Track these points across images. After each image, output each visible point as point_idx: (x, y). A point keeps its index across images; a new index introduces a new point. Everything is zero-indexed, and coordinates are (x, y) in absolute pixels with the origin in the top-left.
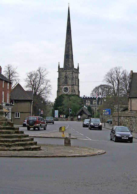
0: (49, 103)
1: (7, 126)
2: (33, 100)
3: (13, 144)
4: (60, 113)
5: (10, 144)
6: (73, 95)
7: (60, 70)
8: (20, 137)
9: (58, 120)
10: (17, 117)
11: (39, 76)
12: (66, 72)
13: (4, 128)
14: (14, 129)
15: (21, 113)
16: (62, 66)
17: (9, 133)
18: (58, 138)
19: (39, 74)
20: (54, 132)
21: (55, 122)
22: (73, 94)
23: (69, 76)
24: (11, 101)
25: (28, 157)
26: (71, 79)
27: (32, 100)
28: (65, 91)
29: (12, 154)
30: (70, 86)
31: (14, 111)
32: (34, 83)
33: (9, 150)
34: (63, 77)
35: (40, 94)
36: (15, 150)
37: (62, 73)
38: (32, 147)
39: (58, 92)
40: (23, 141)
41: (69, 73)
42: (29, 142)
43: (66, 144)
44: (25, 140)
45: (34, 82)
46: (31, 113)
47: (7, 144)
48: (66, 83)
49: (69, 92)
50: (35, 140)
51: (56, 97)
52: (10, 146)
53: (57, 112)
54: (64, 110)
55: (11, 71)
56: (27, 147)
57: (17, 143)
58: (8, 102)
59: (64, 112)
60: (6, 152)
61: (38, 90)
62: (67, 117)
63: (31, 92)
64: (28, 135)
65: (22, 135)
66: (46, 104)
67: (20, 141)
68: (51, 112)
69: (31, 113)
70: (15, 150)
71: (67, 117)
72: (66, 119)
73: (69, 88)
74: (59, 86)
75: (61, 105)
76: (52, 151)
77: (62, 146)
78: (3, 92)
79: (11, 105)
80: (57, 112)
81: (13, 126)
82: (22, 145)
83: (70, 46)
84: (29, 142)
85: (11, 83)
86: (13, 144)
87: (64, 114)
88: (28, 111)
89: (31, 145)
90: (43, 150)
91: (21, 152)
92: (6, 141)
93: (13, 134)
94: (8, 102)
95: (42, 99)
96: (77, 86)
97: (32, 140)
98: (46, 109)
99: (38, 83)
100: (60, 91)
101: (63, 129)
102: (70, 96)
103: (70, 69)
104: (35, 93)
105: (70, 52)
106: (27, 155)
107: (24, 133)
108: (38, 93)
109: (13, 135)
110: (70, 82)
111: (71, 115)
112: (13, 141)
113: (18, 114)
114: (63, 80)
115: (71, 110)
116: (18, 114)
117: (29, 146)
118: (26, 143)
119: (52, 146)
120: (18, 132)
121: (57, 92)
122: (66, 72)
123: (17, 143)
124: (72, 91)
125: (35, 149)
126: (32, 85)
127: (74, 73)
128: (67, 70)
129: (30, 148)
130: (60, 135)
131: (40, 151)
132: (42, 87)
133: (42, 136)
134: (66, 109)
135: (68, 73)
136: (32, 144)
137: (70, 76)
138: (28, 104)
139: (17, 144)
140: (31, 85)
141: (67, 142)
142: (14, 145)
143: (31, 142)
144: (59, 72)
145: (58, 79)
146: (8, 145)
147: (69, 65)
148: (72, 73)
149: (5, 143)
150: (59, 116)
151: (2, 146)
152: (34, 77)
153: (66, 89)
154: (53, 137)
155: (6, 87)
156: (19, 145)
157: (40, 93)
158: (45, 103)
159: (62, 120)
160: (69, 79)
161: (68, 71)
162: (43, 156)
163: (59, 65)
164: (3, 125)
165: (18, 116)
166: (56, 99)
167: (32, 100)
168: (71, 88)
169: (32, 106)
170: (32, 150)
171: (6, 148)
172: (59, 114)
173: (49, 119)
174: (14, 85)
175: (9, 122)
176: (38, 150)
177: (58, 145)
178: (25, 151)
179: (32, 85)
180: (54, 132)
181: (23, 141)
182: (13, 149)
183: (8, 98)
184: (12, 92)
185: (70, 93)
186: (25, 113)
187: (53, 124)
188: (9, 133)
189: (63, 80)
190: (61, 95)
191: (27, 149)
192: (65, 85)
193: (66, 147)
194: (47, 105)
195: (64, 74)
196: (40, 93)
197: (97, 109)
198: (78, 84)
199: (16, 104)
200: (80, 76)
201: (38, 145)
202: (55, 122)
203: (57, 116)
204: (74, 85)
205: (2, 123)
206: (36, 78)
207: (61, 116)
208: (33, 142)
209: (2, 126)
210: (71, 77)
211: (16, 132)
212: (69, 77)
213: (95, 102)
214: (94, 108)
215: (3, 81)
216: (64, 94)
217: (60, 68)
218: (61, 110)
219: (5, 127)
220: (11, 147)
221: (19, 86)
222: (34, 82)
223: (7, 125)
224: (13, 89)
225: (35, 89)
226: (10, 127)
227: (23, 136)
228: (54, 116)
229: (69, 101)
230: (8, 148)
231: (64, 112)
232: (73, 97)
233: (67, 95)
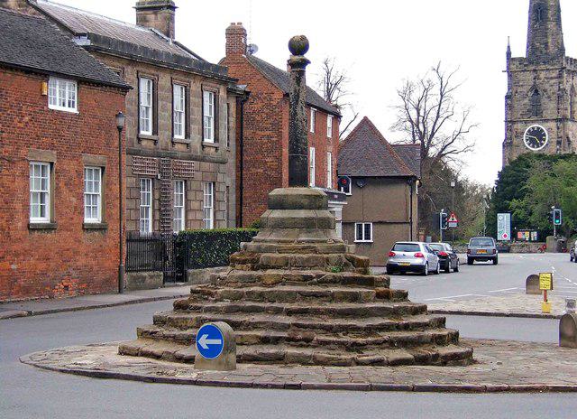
0: (474, 189)
1: (347, 274)
2: (418, 177)
3: (370, 339)
4: (516, 225)
5: (360, 340)
6: (565, 157)
7: (514, 67)
8: (395, 313)
9: (508, 251)
10: (363, 240)
11: (436, 90)
12: (535, 70)
13: (334, 281)
14: (370, 282)
15: (377, 226)
16: (520, 51)
17: (355, 298)
18: (525, 316)
19: (436, 81)
20: (506, 295)
21: (501, 257)
22: (563, 153)
23: (547, 86)
24: (341, 182)
25: (429, 391)
27: (416, 178)
28: (533, 142)
29: (371, 379)
30: (553, 125)
31: (351, 219)
32: (419, 115)
33: (358, 363)
34: (525, 90)
35: (441, 155)
36: (379, 363)
37: (521, 76)
38: (445, 351)
39: (507, 145)
40: (406, 327)
41: (547, 77)
42: (430, 333)
43: (564, 342)
44: (416, 323)
45: (418, 113)
46: (415, 225)
47: (348, 339)
48: (536, 111)
49: (548, 146)
50: (452, 324)
51: (498, 166)
52: (417, 342)
53: (504, 220)
54: (531, 214)
55: (333, 73)
56: (424, 351)
57: (386, 335)
58: (329, 185)
59: (532, 219)
60: (346, 369)
61: (434, 141)
62: (541, 238)
63: (412, 147)
64: (426, 307)
65: (403, 304)
66: (463, 190)
67: (398, 328)
68: (482, 220)
69: (415, 225)
70: (379, 363)
71: (541, 238)
72: (540, 245)
73: (550, 130)
74: (510, 123)
75: (520, 197)
76: (520, 367)
77: (549, 346)
78: (312, 150)
79: (342, 198)
80: (504, 220)
81: (366, 272)
82: (404, 343)
84: (430, 333)
85: (337, 117)
86: (370, 339)
87: (531, 227)
88: (400, 216)
89: (439, 344)
90: (482, 363)
91: (402, 370)
92: (346, 330)
93: (369, 301)
94: (329, 185)
95: (448, 174)
97: (441, 323)
98: (463, 209)
99: (433, 115)
100: (515, 141)
101: (544, 284)
102: (555, 158)
103: (549, 60)
104: (424, 151)
106: (429, 383)
107: (409, 298)
108: (433, 152)
109: (368, 305)
110: (550, 108)
111: (560, 231)
112: (370, 330)
113: (367, 227)
114: (526, 101)
115: (557, 214)
116: (367, 227)
117: (431, 347)
118: (420, 337)
119: (513, 346)
120: (386, 296)
122: (535, 70)
123: (386, 335)
124: (559, 143)
125: (456, 359)
126: (411, 121)
127: (565, 75)
128: (538, 64)
129: (437, 356)
130: (534, 304)
131: (472, 368)
132: (446, 130)
133: (467, 309)
134: (537, 209)
135: (542, 75)
136: (440, 341)
137: (551, 87)
138: (401, 190)
139: (385, 342)
140: (409, 124)
141: (569, 332)
142: (375, 343)
143: (437, 332)
145: (507, 97)
146: (355, 344)
147: (546, 44)
148: (560, 76)
149: (341, 334)
150: (514, 235)
151: (332, 346)
152: (416, 96)
153: (537, 136)
154: (506, 311)
155: (321, 129)
156: (391, 344)
157: (443, 150)
158: (460, 187)
159: (525, 248)
160: (549, 97)
161: (543, 67)
162: (490, 385)
163: (509, 47)
164: (333, 261)
165: (368, 237)
166: (500, 174)
167: (416, 178)
168: (555, 130)
169: (415, 200)
170: (444, 364)
171: (346, 356)
172: (512, 227)
173: (482, 245)
174: (347, 125)
175: (351, 257)
176: (465, 361)
177: (534, 345)
178: (418, 368)
179: (411, 121)
180: (506, 295)
181: (406, 327)
182: (372, 358)
183: (329, 169)
184: (343, 148)
185: (554, 151)
186: (392, 226)
187: (495, 263)
188: (355, 298)
189: (526, 101)
190: (520, 158)
191: (423, 361)
192: (533, 122)
193: (568, 352)
194: (468, 196)
196: (443, 150)
199: (359, 192)
201: (465, 344)
202: (501, 257)
203: (505, 236)
205: (327, 260)
206: (424, 97)
207: (520, 235)
208: (445, 333)
209: (328, 274)
210: (556, 88)
211: (380, 296)
215: (313, 110)
216: (529, 155)
217: (514, 59)
218: (522, 214)
219: (339, 274)
220: (366, 353)
221: (366, 126)
222: (418, 110)
223: (343, 266)
224: (348, 140)
225: (422, 138)
226: (358, 275)
227: (405, 309)
228: (494, 235)
229: (550, 179)
230: (355, 355)
231: (532, 219)
232: (563, 164)
233: (540, 156)
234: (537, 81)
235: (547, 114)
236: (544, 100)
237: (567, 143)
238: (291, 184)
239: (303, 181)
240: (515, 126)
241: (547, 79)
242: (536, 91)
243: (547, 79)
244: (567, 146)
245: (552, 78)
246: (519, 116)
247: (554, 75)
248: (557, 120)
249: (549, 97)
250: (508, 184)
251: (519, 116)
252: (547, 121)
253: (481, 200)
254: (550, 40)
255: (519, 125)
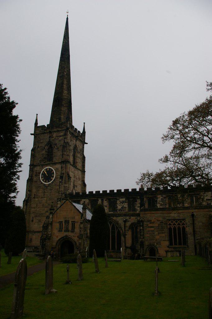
10: (182, 246)
16: (45, 121)
23: (57, 142)
26: (60, 148)
34: (43, 145)
83: (65, 82)
96: (80, 172)
100: (35, 179)
105: (65, 92)
110: (58, 155)
114: (44, 152)
121: (28, 181)
144: (35, 134)
145: (32, 150)
148: (65, 134)
160: (58, 148)
163: (37, 120)
168: (60, 169)
189: (44, 152)
195: (46, 137)
197: (128, 224)
198: (83, 166)
200: (88, 151)
204: (69, 162)
210: (62, 142)
212: (56, 144)
213: (123, 202)
214: (120, 220)
234: (51, 139)
235: (55, 160)
236: (55, 150)
237: (67, 178)
238: (183, 245)
239: (172, 245)
240: (36, 169)
241: (57, 136)
242: (51, 146)
243: (57, 136)
244: (67, 180)
245: (60, 136)
246: (39, 162)
247: (62, 134)
248: (60, 163)
249: (58, 148)
250: (199, 111)
251: (39, 162)
252: (55, 164)
253: (30, 210)
254: (62, 117)
255: (38, 167)
